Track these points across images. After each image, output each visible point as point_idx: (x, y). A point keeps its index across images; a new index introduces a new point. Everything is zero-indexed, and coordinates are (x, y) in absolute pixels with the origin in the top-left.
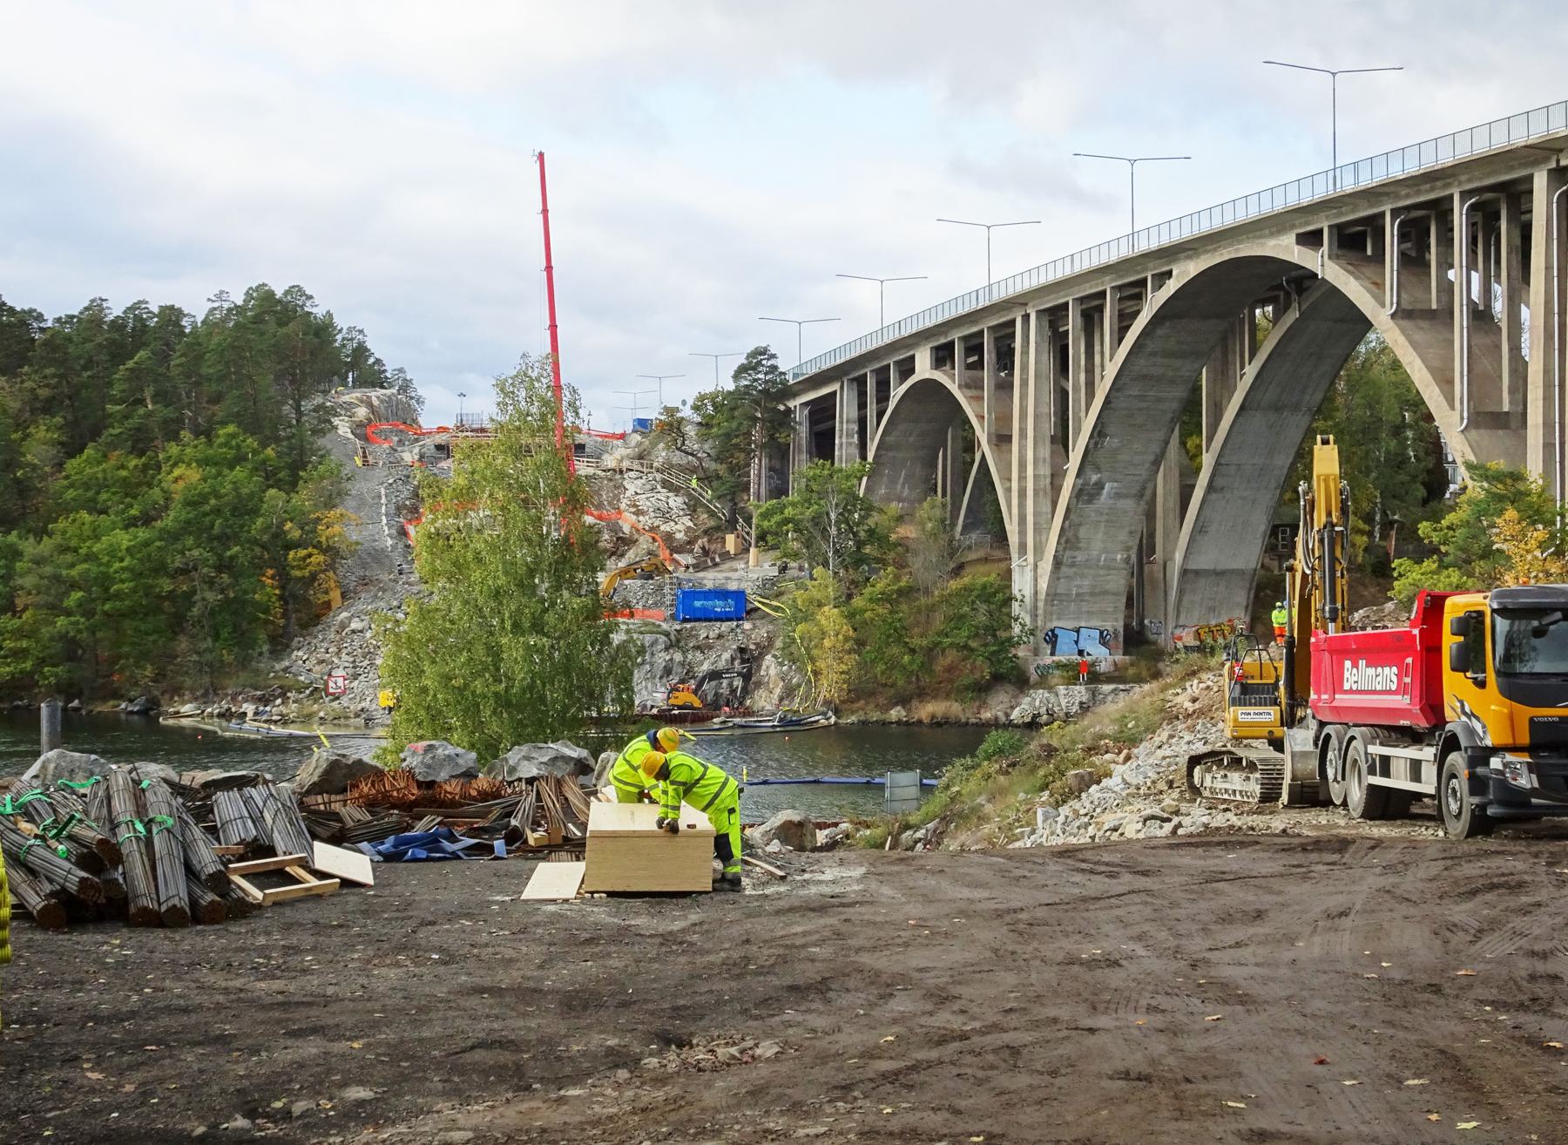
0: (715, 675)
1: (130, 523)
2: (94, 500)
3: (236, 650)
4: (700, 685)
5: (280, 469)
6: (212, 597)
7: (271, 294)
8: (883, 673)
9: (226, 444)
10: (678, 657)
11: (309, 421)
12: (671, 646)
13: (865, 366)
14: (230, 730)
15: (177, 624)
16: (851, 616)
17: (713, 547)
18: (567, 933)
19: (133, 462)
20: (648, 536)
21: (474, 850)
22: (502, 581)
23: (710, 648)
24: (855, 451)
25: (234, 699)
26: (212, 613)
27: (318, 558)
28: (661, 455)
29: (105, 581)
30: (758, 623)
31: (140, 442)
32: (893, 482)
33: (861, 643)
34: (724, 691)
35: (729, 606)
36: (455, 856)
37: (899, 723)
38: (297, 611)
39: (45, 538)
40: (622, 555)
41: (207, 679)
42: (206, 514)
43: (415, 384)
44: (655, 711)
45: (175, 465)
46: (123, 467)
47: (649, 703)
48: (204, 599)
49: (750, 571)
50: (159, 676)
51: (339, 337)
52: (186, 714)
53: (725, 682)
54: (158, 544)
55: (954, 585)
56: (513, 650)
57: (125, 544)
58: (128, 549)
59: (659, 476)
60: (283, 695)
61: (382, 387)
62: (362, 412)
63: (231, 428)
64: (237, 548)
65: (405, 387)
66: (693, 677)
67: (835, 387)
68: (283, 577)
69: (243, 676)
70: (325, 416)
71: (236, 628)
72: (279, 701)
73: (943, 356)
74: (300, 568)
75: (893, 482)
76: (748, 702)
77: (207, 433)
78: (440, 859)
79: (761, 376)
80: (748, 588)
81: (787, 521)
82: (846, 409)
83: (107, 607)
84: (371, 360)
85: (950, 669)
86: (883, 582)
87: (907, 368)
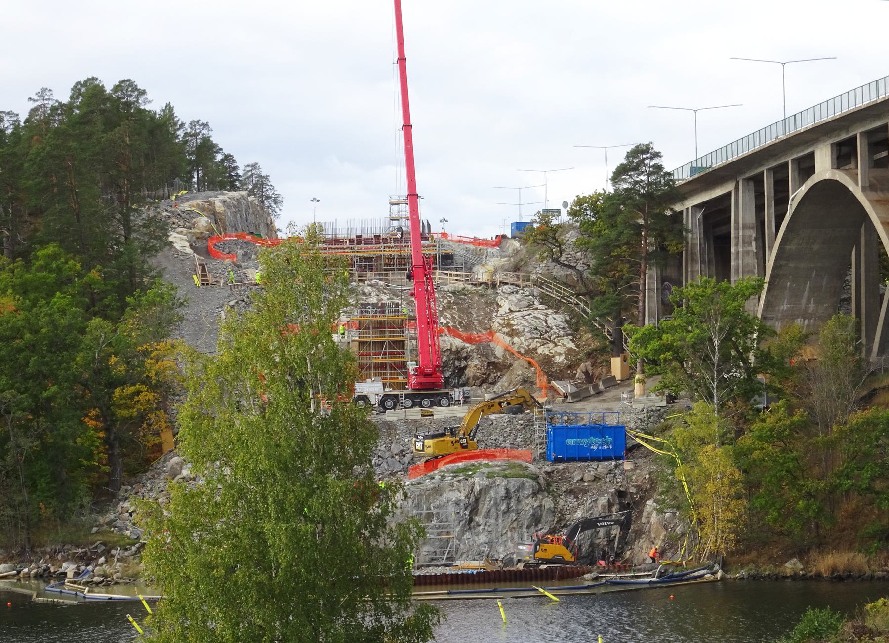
0: (588, 524)
3: (54, 502)
4: (571, 536)
6: (25, 442)
7: (102, 89)
8: (775, 520)
9: (45, 267)
10: (548, 503)
13: (761, 165)
16: (740, 455)
17: (597, 372)
20: (523, 361)
22: (265, 465)
23: (585, 491)
24: (752, 261)
25: (53, 558)
26: (28, 461)
27: (147, 395)
28: (539, 269)
30: (640, 462)
32: (796, 296)
33: (752, 487)
34: (601, 539)
35: (606, 444)
37: (794, 577)
38: (124, 455)
40: (494, 383)
41: (24, 536)
42: (20, 350)
43: (272, 181)
44: (520, 567)
48: (18, 446)
49: (632, 402)
51: (181, 133)
53: (602, 532)
55: (857, 417)
56: (277, 534)
59: (537, 291)
60: (107, 552)
61: (233, 188)
62: (203, 222)
63: (51, 249)
64: (54, 389)
65: (260, 185)
66: (565, 526)
67: (729, 187)
68: (108, 419)
70: (159, 231)
72: (102, 559)
73: (844, 155)
74: (128, 407)
75: (796, 296)
76: (628, 554)
79: (643, 178)
80: (630, 421)
81: (668, 348)
82: (742, 213)
84: (219, 157)
85: (854, 515)
86: (774, 416)
87: (806, 167)
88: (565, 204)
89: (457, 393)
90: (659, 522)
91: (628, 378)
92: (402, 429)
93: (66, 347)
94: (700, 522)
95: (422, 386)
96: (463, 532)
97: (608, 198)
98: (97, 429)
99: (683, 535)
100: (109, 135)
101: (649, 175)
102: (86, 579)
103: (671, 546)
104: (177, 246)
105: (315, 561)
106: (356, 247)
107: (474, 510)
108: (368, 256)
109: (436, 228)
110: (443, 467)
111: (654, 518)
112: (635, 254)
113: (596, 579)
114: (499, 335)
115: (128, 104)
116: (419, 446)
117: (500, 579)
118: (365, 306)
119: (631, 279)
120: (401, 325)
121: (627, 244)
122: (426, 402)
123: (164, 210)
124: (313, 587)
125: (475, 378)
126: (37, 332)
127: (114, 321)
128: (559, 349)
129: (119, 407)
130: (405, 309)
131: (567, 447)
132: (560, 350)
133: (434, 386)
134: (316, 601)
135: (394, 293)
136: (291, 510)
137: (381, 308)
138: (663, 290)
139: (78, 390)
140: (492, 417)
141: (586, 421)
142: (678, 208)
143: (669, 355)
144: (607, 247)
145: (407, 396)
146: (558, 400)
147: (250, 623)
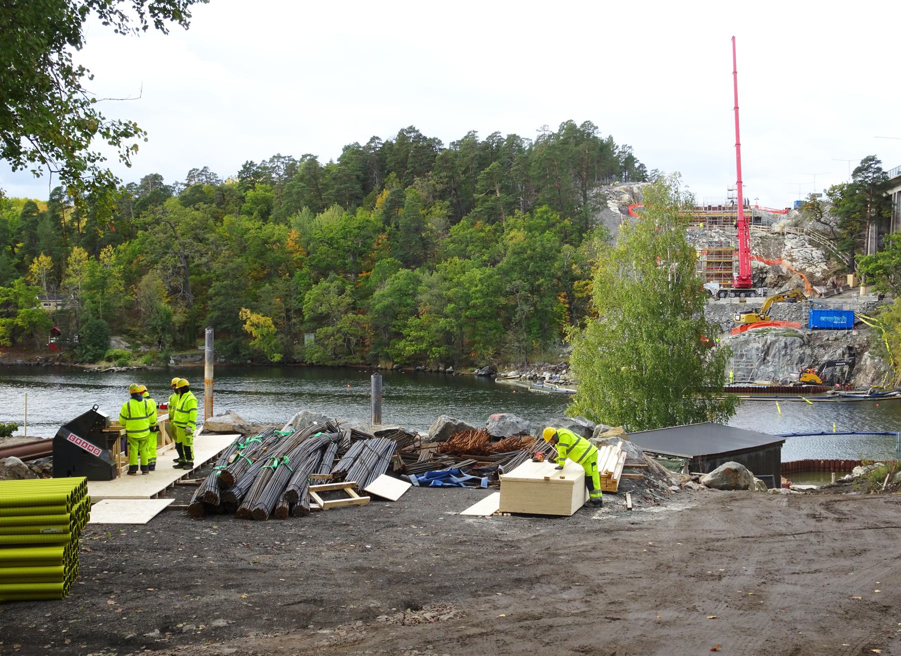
0: (831, 364)
1: (485, 264)
2: (464, 250)
3: (540, 340)
4: (821, 369)
5: (572, 232)
6: (526, 308)
7: (575, 126)
9: (541, 217)
10: (808, 351)
11: (591, 203)
12: (804, 344)
14: (535, 388)
15: (507, 324)
18: (478, 537)
19: (488, 228)
21: (470, 483)
22: (641, 309)
23: (830, 346)
28: (809, 225)
29: (467, 297)
30: (862, 331)
31: (493, 216)
34: (838, 373)
35: (843, 320)
36: (458, 485)
39: (435, 273)
40: (781, 287)
42: (525, 260)
44: (791, 385)
45: (511, 230)
46: (482, 231)
47: (789, 380)
49: (859, 298)
50: (497, 354)
51: (617, 151)
52: (511, 377)
53: (838, 369)
54: (497, 277)
57: (478, 277)
58: (480, 280)
59: (807, 237)
61: (644, 181)
62: (626, 197)
63: (544, 208)
64: (541, 280)
68: (570, 297)
69: (544, 356)
70: (602, 201)
71: (541, 327)
72: (564, 371)
77: (530, 211)
78: (449, 487)
79: (870, 174)
80: (857, 309)
81: (880, 267)
83: (468, 313)
84: (637, 165)
88: (825, 190)
89: (760, 291)
90: (871, 364)
91: (856, 287)
92: (729, 308)
93: (549, 259)
94: (895, 365)
95: (741, 286)
96: (760, 365)
97: (850, 186)
98: (564, 303)
99: (885, 372)
100: (577, 148)
101: (874, 173)
102: (555, 381)
103: (878, 378)
104: (612, 209)
105: (668, 366)
106: (708, 211)
107: (767, 353)
108: (715, 218)
109: (752, 203)
110: (750, 329)
111: (868, 362)
112: (864, 217)
113: (834, 394)
114: (785, 261)
115: (589, 134)
116: (738, 318)
117: (780, 391)
118: (711, 242)
119: (861, 231)
120: (731, 253)
121: (859, 211)
122: (743, 295)
123: (604, 190)
124: (666, 381)
125: (771, 284)
126: (534, 250)
127: (576, 247)
128: (818, 269)
129: (577, 292)
130: (733, 245)
131: (821, 321)
132: (819, 269)
133: (748, 286)
134: (668, 389)
135: (728, 237)
136: (655, 336)
137: (720, 244)
138: (879, 238)
139: (555, 281)
140: (779, 304)
141: (832, 308)
142: (890, 192)
143: (881, 271)
144: (848, 213)
145: (732, 291)
146: (816, 296)
147: (630, 400)
